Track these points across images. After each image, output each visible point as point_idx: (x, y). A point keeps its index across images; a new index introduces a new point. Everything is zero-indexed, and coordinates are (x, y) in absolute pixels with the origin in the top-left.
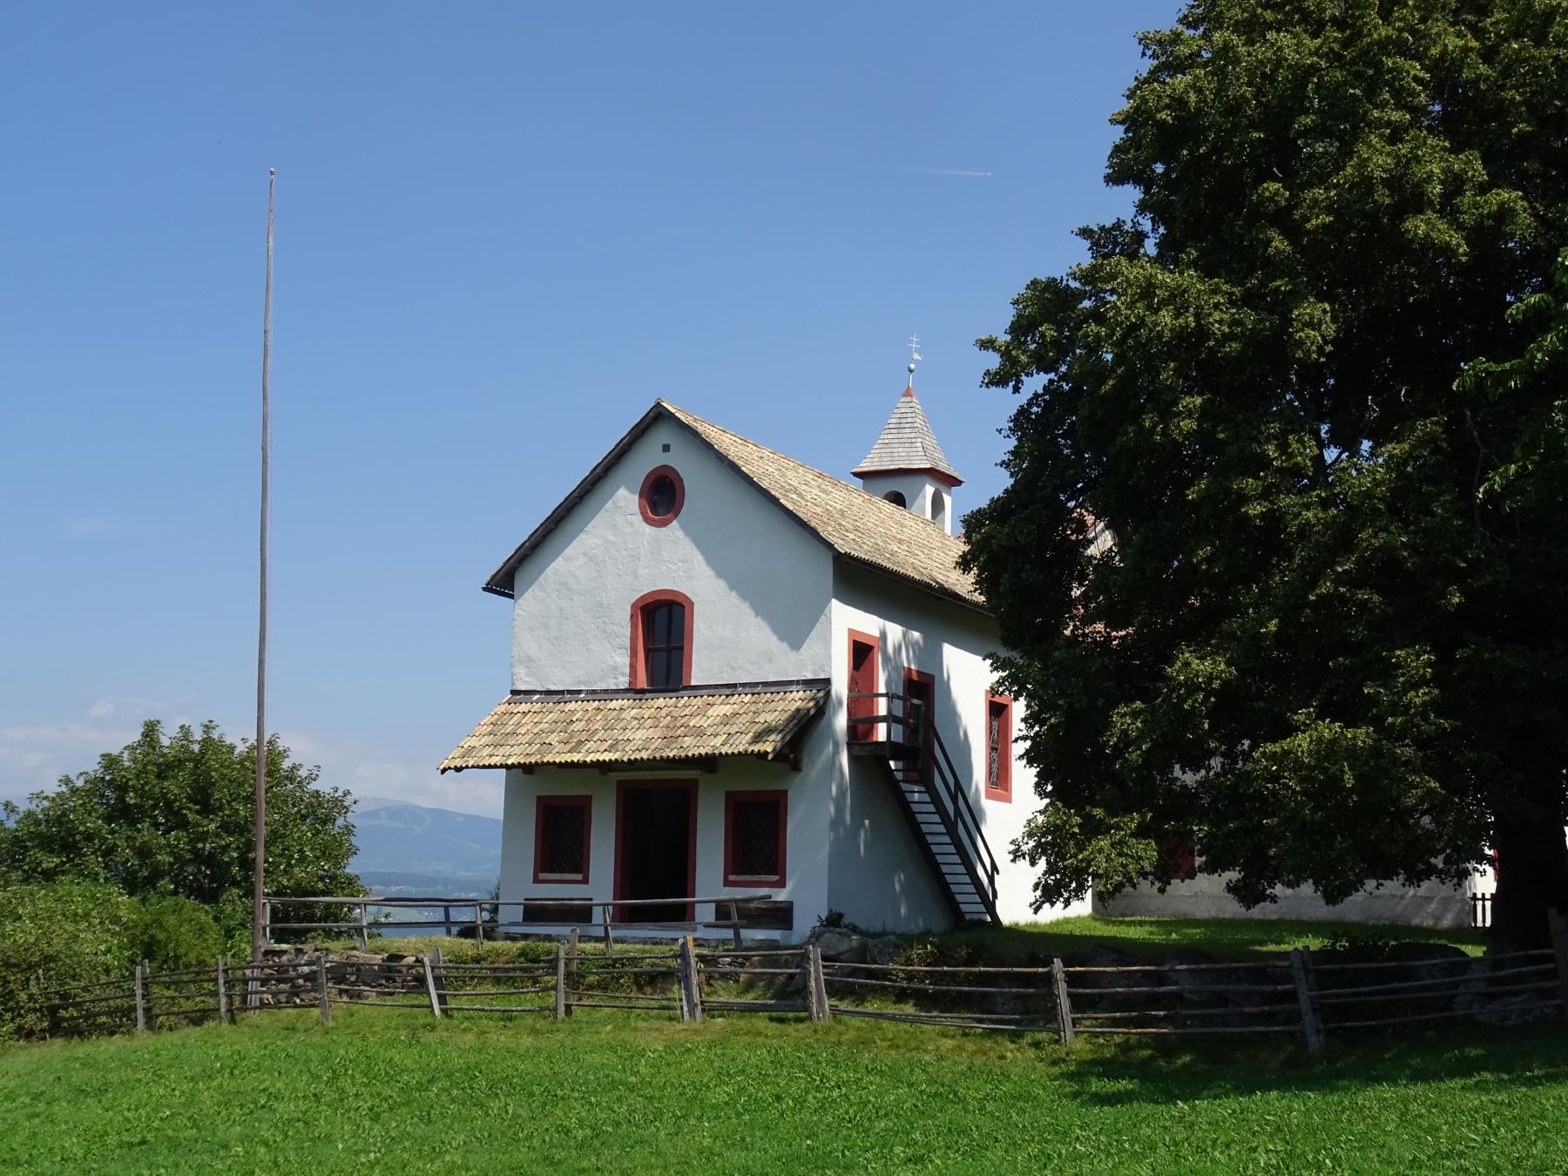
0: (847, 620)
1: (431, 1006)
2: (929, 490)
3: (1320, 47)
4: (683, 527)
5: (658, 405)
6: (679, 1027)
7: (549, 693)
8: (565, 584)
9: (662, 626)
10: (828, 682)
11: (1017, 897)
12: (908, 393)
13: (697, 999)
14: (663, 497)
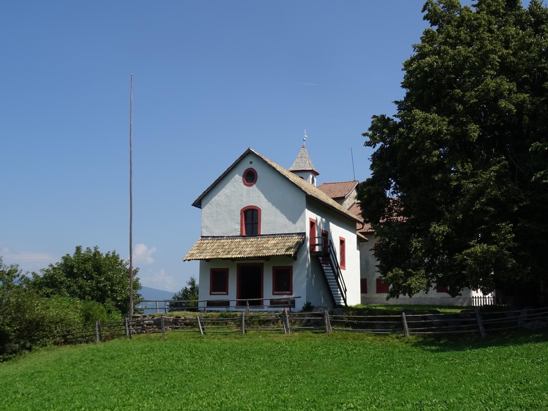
0: (310, 215)
1: (200, 332)
2: (311, 176)
3: (472, 51)
4: (258, 187)
5: (249, 149)
6: (284, 335)
7: (214, 237)
8: (218, 204)
9: (251, 218)
10: (305, 233)
11: (353, 297)
12: (303, 147)
13: (289, 327)
14: (250, 177)
